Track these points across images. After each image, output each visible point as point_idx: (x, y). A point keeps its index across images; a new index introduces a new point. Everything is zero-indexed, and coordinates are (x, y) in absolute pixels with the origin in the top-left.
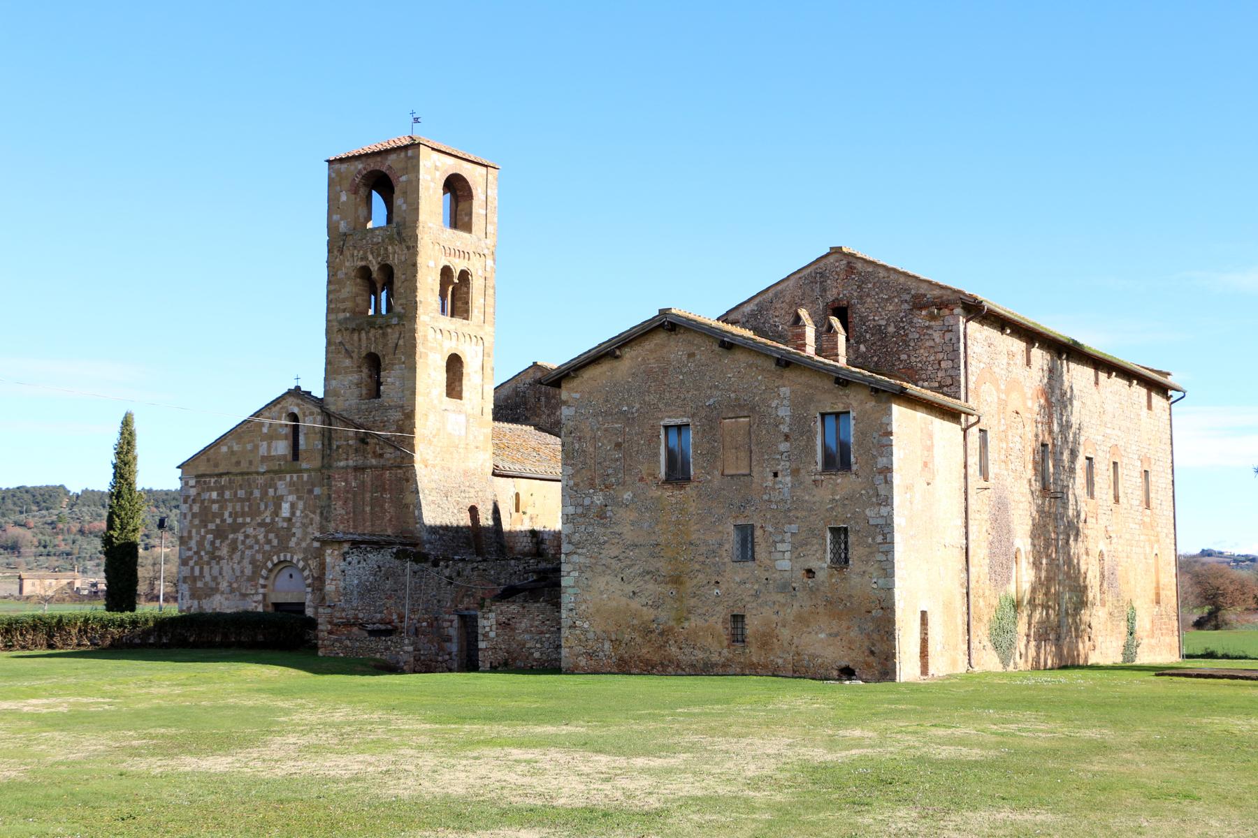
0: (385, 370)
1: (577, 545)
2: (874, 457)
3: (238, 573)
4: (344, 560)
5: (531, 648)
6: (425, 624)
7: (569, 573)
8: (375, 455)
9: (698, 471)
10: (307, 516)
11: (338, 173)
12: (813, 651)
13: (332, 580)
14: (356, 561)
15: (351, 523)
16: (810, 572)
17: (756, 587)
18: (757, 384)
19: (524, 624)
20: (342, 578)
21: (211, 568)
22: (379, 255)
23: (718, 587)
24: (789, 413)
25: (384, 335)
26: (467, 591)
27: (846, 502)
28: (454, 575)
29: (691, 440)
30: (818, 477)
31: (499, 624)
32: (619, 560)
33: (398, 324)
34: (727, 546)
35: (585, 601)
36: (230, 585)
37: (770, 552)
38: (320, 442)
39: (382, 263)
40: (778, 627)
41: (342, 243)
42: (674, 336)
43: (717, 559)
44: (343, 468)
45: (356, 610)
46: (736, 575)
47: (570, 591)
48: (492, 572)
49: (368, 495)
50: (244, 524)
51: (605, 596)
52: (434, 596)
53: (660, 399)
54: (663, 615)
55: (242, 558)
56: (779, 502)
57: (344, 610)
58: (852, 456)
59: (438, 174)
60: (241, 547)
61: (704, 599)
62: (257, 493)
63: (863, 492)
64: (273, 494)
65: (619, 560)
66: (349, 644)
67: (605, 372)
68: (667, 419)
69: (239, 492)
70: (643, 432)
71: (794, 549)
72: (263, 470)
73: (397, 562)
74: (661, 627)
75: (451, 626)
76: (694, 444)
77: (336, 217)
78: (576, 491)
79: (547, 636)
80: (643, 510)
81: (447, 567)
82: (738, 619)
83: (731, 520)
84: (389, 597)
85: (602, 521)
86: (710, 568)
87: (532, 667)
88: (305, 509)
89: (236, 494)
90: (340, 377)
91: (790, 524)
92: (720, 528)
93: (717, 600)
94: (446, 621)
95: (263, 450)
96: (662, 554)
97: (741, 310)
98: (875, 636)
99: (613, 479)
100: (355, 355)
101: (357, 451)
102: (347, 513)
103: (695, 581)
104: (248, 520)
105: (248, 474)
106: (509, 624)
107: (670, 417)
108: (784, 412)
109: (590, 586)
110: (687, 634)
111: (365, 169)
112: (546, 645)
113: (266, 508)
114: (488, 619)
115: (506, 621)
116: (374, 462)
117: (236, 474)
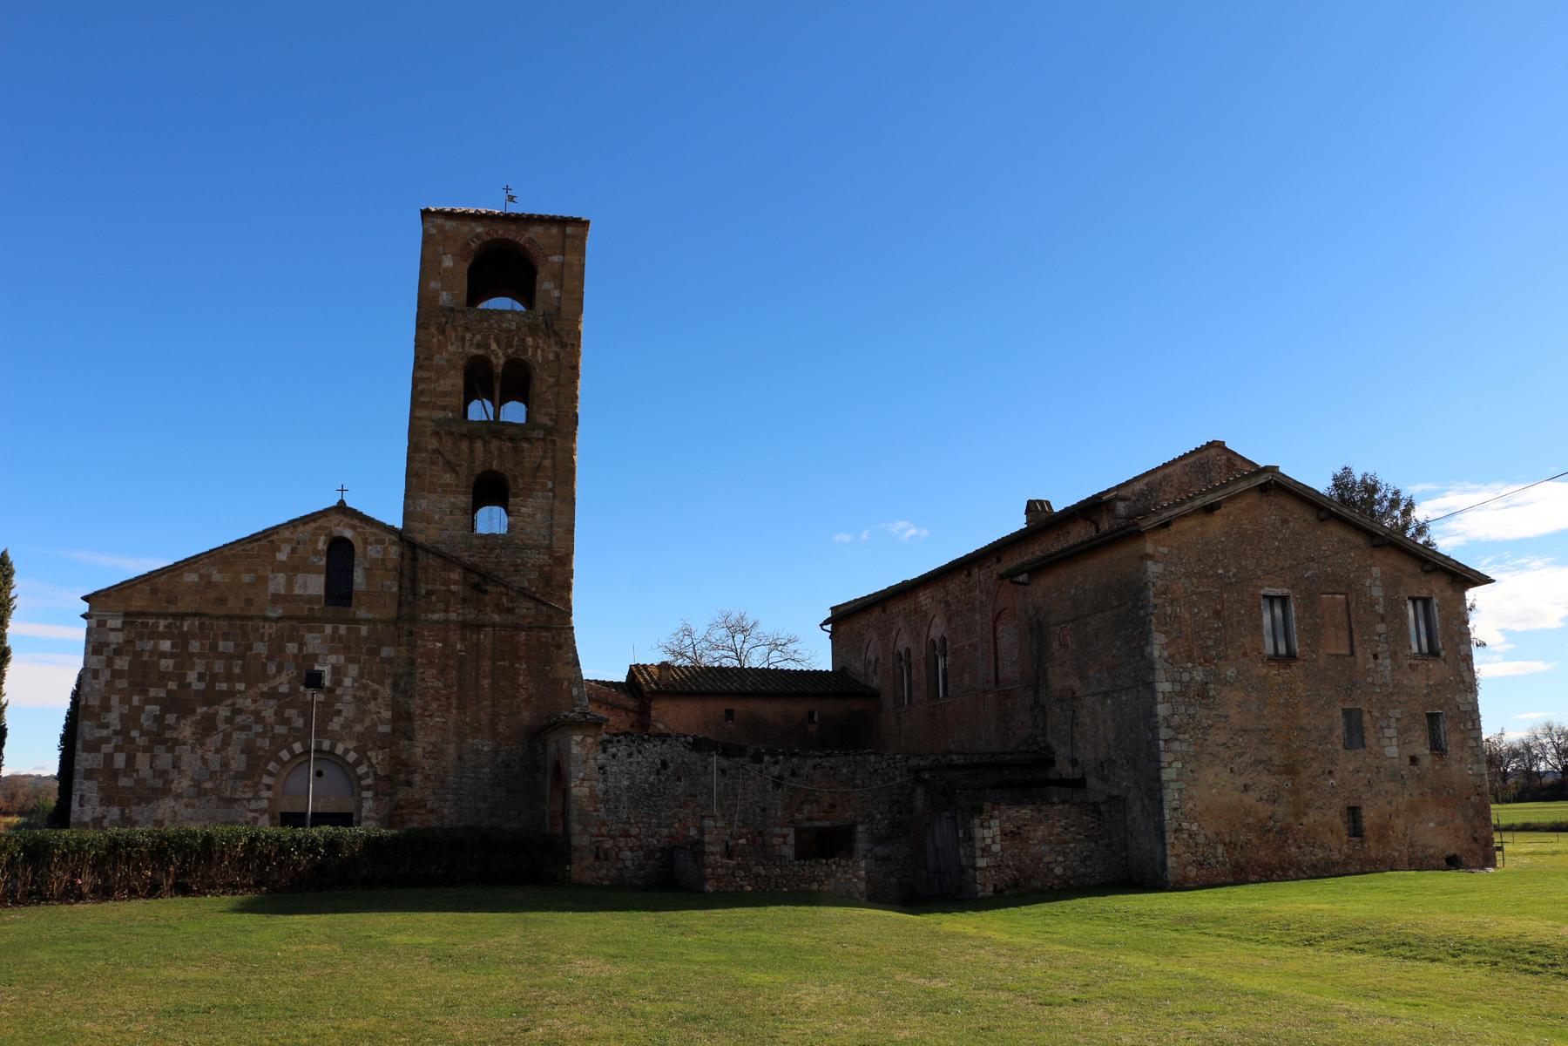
0: (517, 495)
1: (1178, 729)
3: (216, 766)
4: (604, 751)
5: (1050, 863)
6: (742, 841)
7: (1170, 764)
8: (499, 608)
9: (1303, 649)
10: (365, 687)
11: (441, 229)
12: (1425, 841)
13: (583, 780)
14: (625, 753)
15: (454, 701)
16: (1414, 760)
17: (1368, 776)
18: (1350, 560)
19: (1042, 831)
20: (601, 777)
21: (153, 758)
22: (509, 345)
23: (1333, 777)
24: (1381, 594)
25: (517, 450)
26: (808, 795)
27: (1439, 688)
28: (787, 774)
29: (1294, 614)
30: (1413, 662)
31: (1004, 834)
32: (1228, 747)
33: (543, 439)
35: (1191, 798)
36: (197, 784)
37: (1379, 739)
38: (396, 584)
39: (513, 356)
40: (1393, 818)
41: (444, 319)
42: (1265, 498)
43: (1329, 746)
44: (438, 622)
45: (625, 823)
47: (1174, 786)
48: (844, 771)
49: (486, 665)
51: (1214, 791)
52: (757, 802)
54: (1280, 811)
55: (226, 742)
56: (1382, 685)
57: (604, 824)
58: (1440, 642)
60: (222, 727)
61: (1320, 790)
62: (261, 648)
63: (1452, 678)
64: (296, 651)
65: (1228, 747)
66: (763, 872)
67: (1195, 527)
68: (1267, 589)
69: (221, 644)
70: (1243, 600)
71: (1400, 736)
72: (275, 615)
73: (695, 756)
74: (1279, 824)
75: (785, 843)
76: (1297, 618)
77: (434, 285)
78: (1172, 664)
79: (1072, 846)
80: (1250, 690)
81: (776, 763)
82: (1354, 813)
83: (1339, 704)
84: (684, 805)
85: (1204, 701)
86: (1324, 756)
87: (1051, 887)
88: (361, 675)
89: (214, 647)
90: (433, 496)
91: (1394, 708)
92: (1330, 712)
93: (1333, 791)
94: (776, 836)
95: (277, 583)
96: (1273, 741)
97: (1130, 488)
98: (1476, 822)
99: (1214, 653)
100: (463, 470)
101: (464, 600)
102: (446, 687)
104: (241, 686)
106: (1019, 834)
107: (1269, 586)
108: (1377, 592)
109: (1197, 780)
110: (1307, 831)
111: (487, 234)
112: (1071, 857)
114: (990, 827)
115: (1015, 829)
116: (496, 618)
117: (218, 618)
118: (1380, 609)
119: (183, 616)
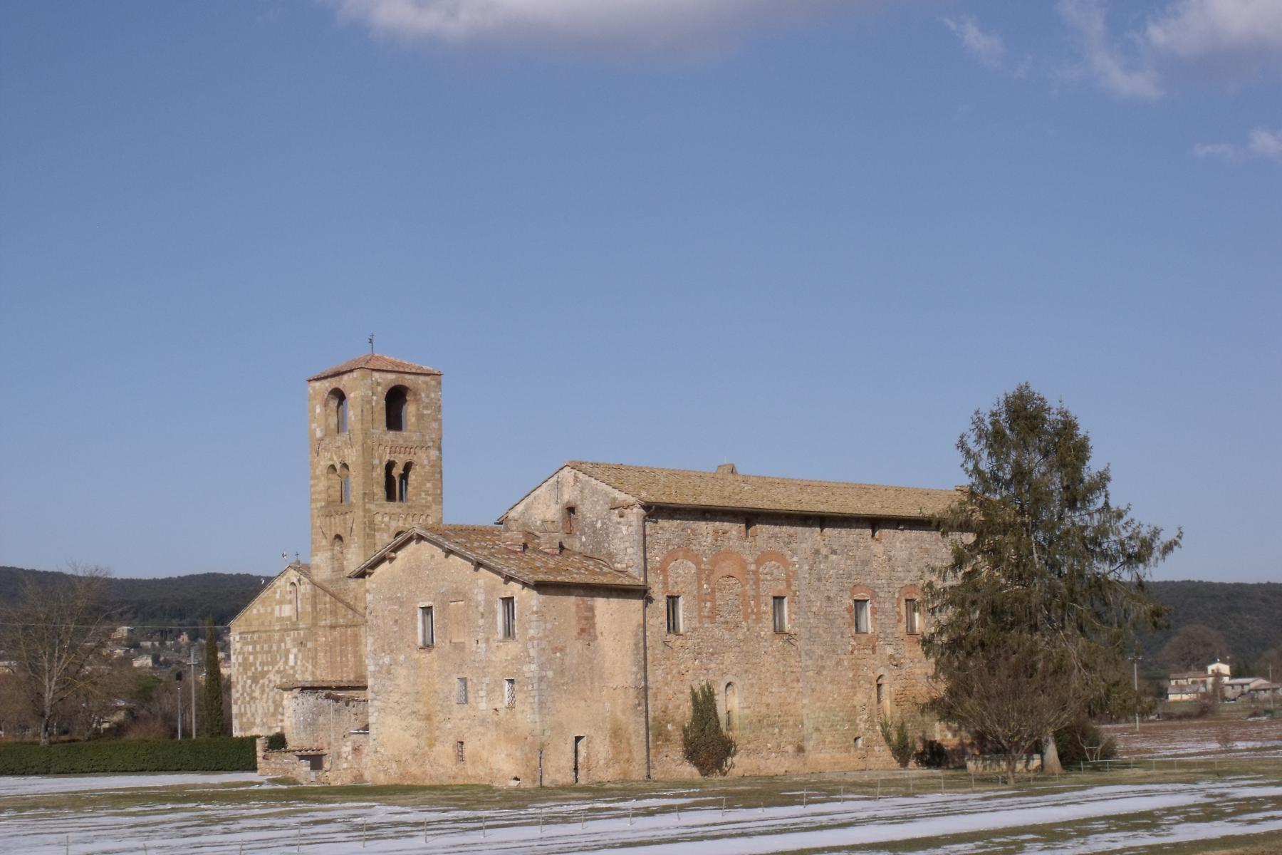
2: (527, 629)
17: (469, 722)
34: (454, 693)
46: (458, 712)
50: (268, 672)
53: (417, 588)
59: (380, 389)
102: (327, 662)
103: (438, 718)
105: (269, 631)
113: (281, 658)
118: (481, 609)
119: (253, 632)
